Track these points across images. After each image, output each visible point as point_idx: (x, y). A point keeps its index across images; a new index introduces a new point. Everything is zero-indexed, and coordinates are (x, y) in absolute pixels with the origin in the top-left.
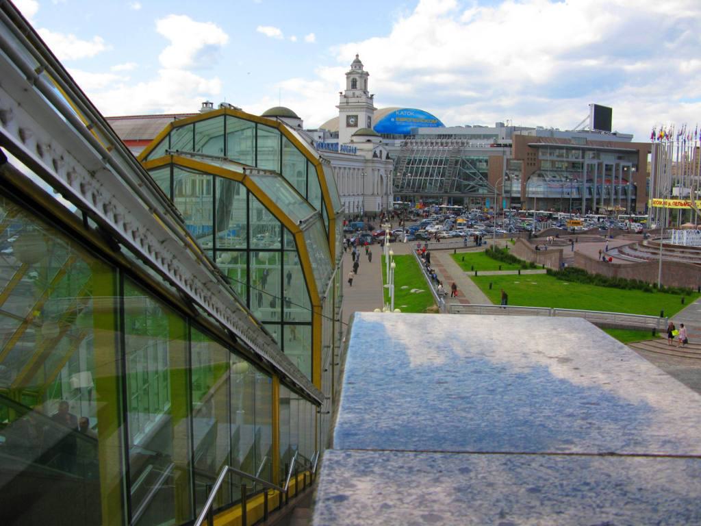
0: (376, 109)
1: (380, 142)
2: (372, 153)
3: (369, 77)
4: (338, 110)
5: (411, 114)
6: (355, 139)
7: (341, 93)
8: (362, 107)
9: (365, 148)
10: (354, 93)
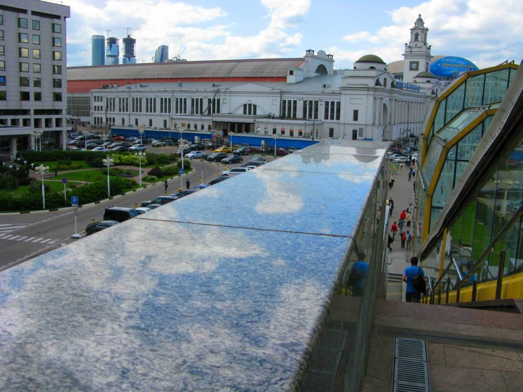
0: (433, 57)
1: (437, 82)
2: (431, 91)
3: (428, 32)
4: (404, 57)
5: (454, 60)
6: (418, 80)
7: (406, 44)
8: (422, 55)
9: (426, 87)
10: (416, 44)
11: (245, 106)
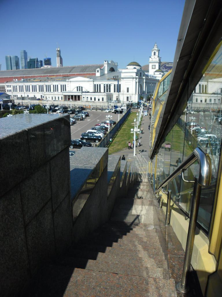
0: (162, 63)
6: (156, 73)
11: (77, 87)
